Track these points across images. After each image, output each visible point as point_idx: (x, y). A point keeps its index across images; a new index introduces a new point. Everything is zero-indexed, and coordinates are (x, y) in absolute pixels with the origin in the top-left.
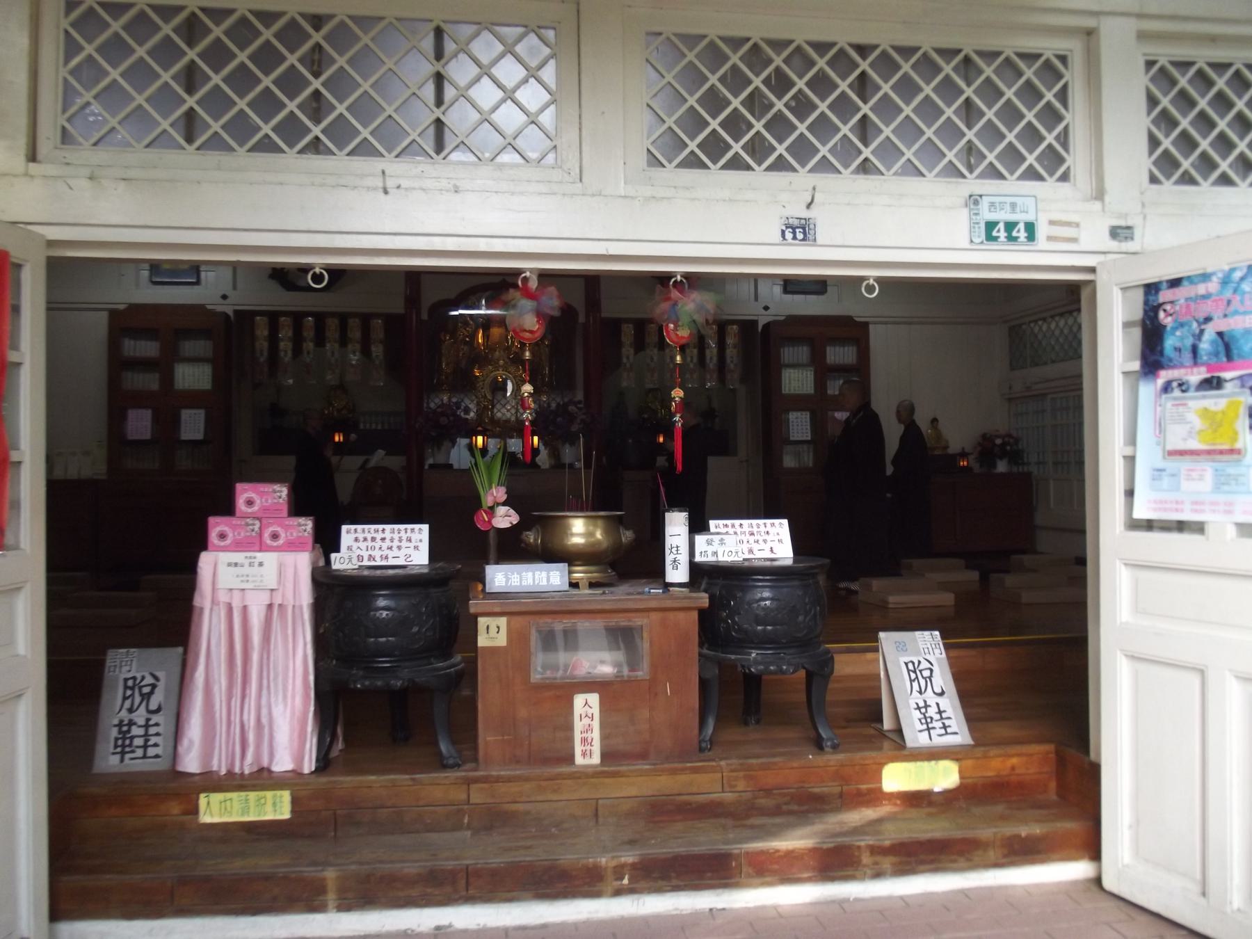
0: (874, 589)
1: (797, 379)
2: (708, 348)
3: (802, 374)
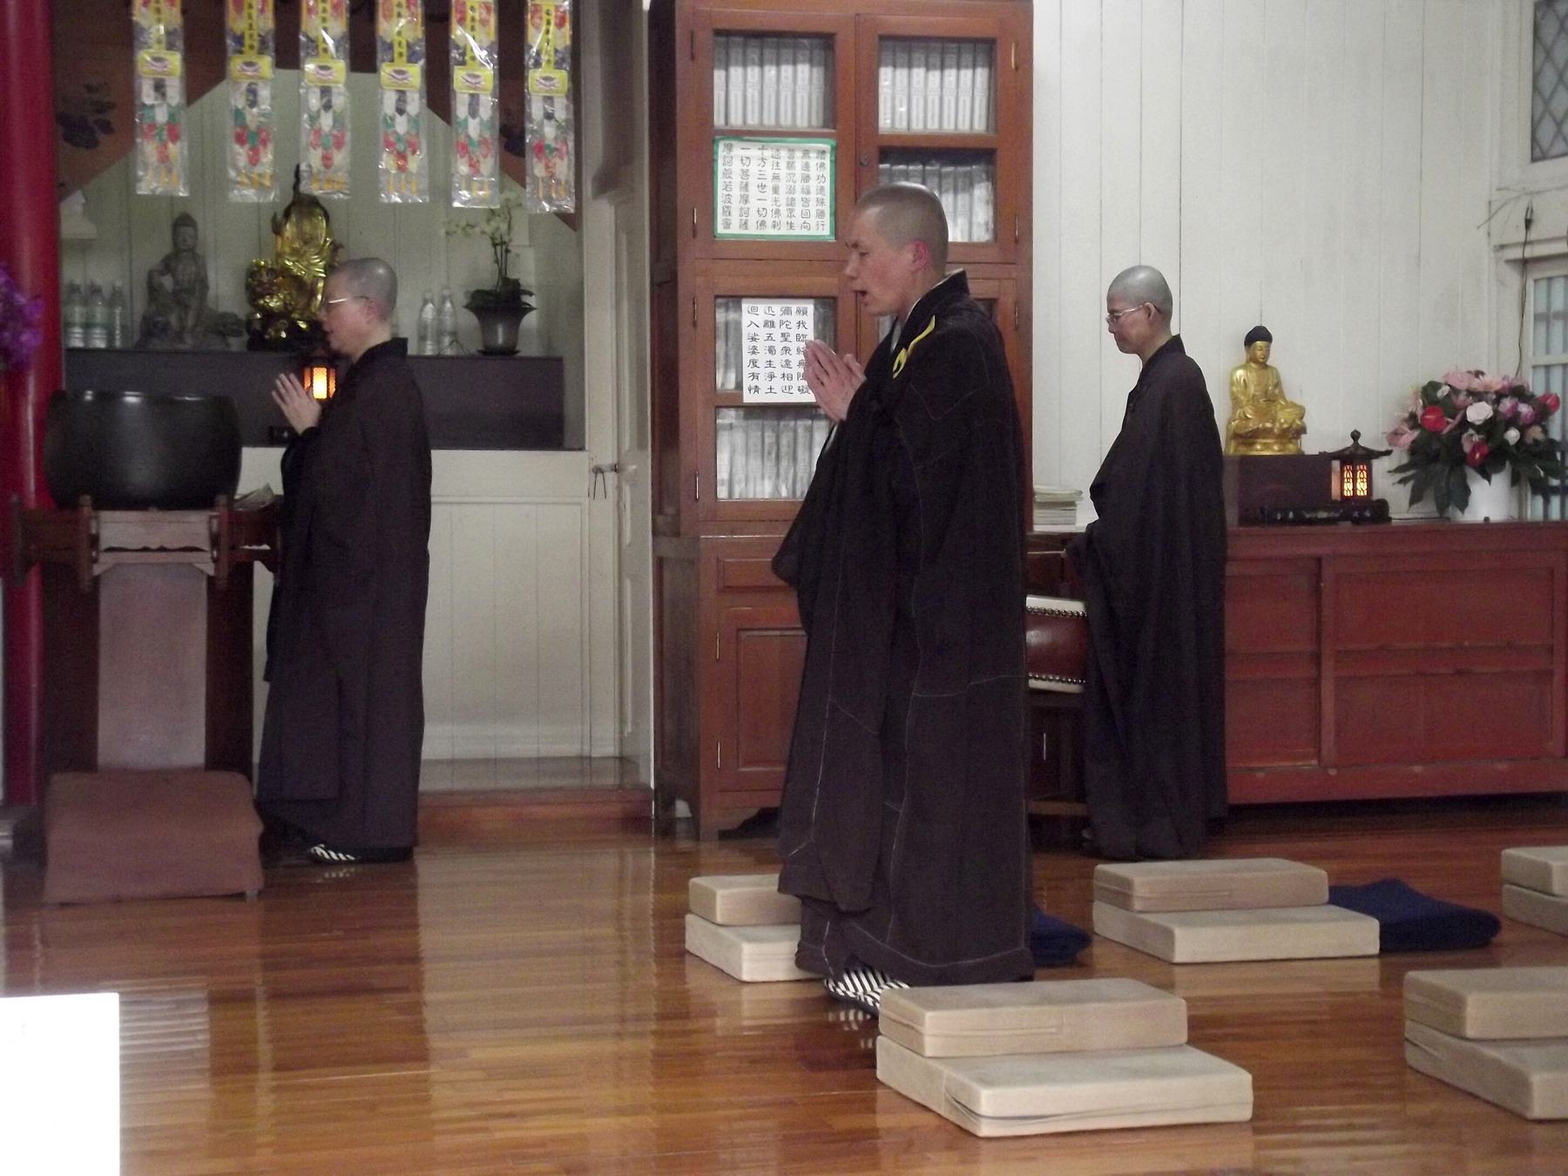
0: (931, 1046)
1: (770, 184)
2: (463, 63)
3: (790, 165)
